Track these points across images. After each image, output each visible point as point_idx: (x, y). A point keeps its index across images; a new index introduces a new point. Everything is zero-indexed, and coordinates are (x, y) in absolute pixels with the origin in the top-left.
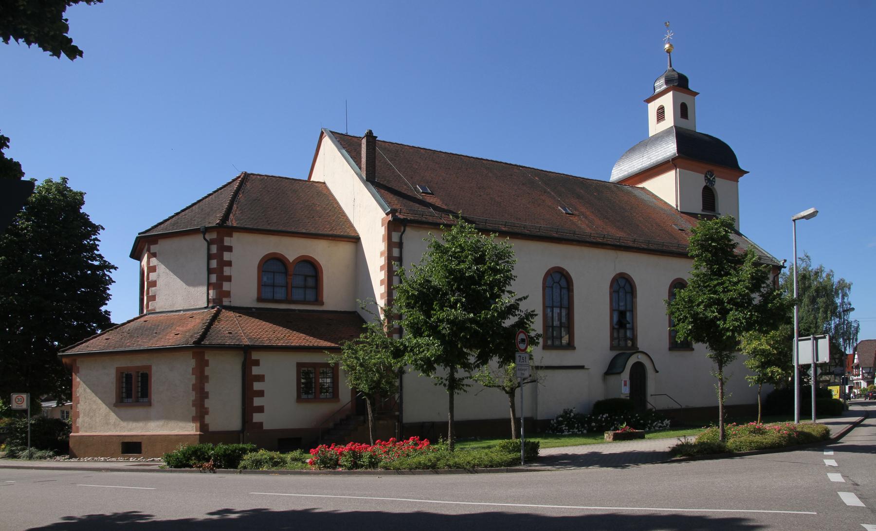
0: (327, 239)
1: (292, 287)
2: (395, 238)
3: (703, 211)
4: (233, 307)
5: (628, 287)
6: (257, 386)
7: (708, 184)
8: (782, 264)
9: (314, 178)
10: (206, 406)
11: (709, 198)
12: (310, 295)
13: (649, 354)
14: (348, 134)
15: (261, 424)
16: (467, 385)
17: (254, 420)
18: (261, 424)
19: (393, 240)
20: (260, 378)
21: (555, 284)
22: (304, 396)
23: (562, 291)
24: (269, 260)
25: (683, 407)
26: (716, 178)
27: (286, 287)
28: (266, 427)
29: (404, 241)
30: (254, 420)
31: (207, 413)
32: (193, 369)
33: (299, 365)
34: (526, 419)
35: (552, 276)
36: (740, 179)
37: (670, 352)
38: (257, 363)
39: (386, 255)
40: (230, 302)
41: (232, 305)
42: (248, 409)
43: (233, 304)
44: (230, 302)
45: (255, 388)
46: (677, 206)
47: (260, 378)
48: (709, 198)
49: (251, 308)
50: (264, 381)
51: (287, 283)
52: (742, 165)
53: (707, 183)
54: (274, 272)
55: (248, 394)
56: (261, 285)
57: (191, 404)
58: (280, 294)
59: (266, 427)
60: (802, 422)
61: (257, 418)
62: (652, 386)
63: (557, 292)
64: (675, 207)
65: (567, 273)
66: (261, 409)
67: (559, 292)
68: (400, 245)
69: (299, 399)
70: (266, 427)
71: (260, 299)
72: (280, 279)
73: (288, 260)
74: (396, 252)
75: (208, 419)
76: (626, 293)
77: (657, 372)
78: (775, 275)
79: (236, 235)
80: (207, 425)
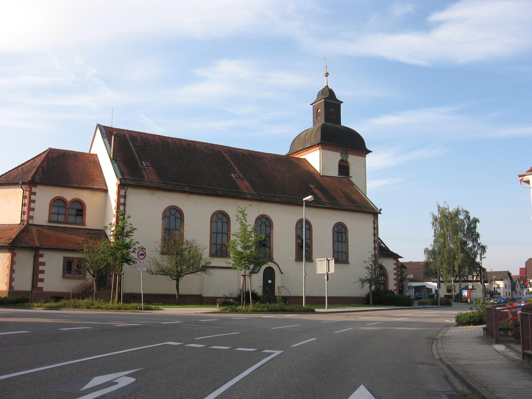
0: (90, 190)
1: (68, 215)
2: (122, 192)
3: (339, 175)
4: (34, 224)
5: (267, 223)
6: (41, 268)
7: (343, 158)
8: (379, 211)
9: (91, 153)
10: (13, 277)
11: (344, 168)
12: (79, 219)
13: (277, 263)
14: (112, 127)
15: (42, 288)
16: (365, 268)
17: (38, 286)
18: (42, 288)
19: (121, 194)
20: (43, 264)
21: (219, 220)
22: (67, 275)
23: (223, 224)
24: (56, 200)
25: (291, 295)
26: (349, 155)
27: (65, 215)
28: (45, 290)
29: (127, 195)
30: (38, 286)
31: (13, 280)
32: (8, 257)
33: (65, 258)
34: (307, 298)
35: (217, 215)
36: (367, 156)
37: (296, 262)
38: (42, 256)
39: (117, 202)
40: (33, 222)
41: (34, 224)
42: (35, 280)
43: (34, 223)
44: (33, 222)
45: (40, 269)
46: (320, 171)
47: (43, 264)
48: (344, 168)
49: (44, 226)
50: (45, 266)
51: (66, 213)
52: (368, 147)
53: (342, 158)
54: (59, 207)
55: (36, 271)
56: (51, 213)
57: (5, 275)
58: (61, 218)
59: (44, 290)
60: (328, 309)
61: (40, 284)
62: (278, 282)
63: (220, 224)
64: (319, 172)
65: (227, 214)
66: (42, 280)
67: (222, 224)
68: (125, 197)
69: (64, 276)
70: (44, 290)
71: (49, 221)
72: (62, 210)
73: (67, 201)
74: (122, 201)
75: (13, 284)
76: (266, 226)
77: (282, 273)
78: (375, 218)
79: (38, 187)
80: (13, 287)
